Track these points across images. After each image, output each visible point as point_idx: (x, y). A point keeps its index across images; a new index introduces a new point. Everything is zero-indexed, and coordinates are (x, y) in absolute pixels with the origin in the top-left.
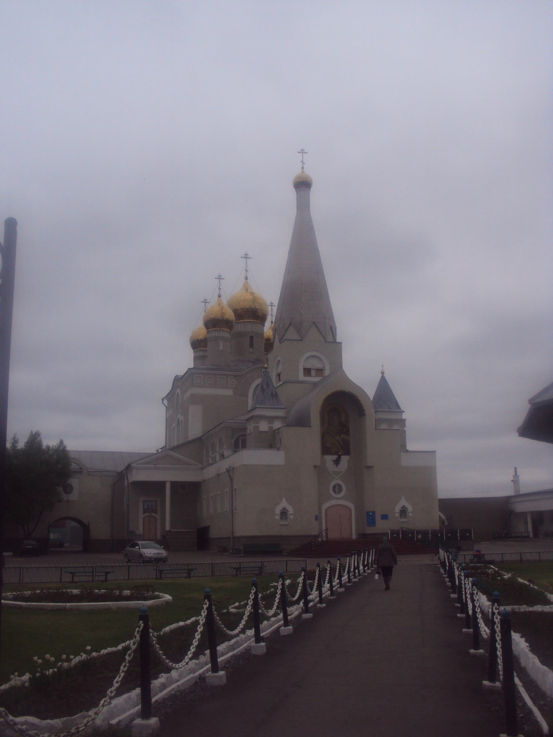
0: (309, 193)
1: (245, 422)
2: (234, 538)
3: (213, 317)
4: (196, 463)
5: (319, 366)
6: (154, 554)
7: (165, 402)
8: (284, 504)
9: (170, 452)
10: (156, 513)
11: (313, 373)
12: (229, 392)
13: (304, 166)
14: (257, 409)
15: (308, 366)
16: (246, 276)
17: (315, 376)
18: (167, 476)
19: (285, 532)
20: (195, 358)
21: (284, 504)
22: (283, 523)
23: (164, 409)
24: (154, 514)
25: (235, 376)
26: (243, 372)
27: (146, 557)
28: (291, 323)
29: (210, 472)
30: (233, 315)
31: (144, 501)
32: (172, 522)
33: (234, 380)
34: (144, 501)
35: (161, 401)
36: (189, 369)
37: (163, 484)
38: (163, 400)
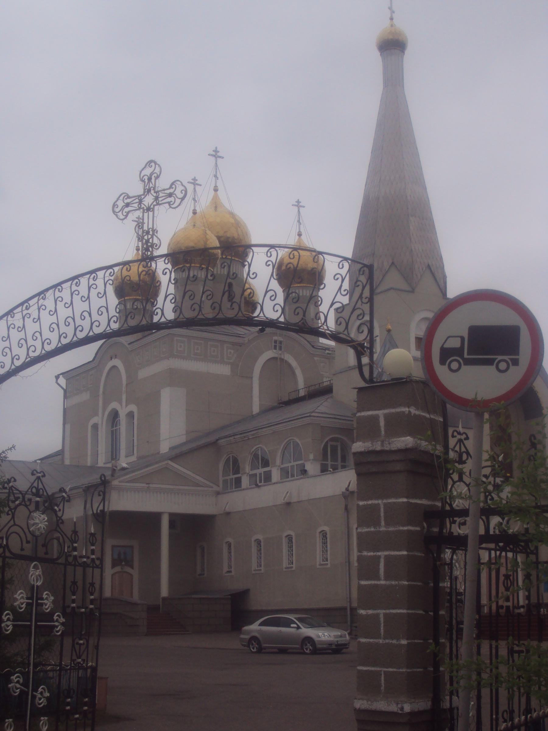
3: (192, 244)
4: (208, 483)
6: (336, 636)
7: (62, 381)
9: (170, 462)
10: (132, 567)
12: (224, 370)
13: (394, 16)
16: (216, 186)
23: (62, 392)
25: (234, 344)
27: (322, 642)
28: (393, 263)
31: (113, 547)
32: (172, 582)
33: (232, 351)
34: (113, 547)
35: (55, 380)
37: (155, 517)
38: (57, 377)
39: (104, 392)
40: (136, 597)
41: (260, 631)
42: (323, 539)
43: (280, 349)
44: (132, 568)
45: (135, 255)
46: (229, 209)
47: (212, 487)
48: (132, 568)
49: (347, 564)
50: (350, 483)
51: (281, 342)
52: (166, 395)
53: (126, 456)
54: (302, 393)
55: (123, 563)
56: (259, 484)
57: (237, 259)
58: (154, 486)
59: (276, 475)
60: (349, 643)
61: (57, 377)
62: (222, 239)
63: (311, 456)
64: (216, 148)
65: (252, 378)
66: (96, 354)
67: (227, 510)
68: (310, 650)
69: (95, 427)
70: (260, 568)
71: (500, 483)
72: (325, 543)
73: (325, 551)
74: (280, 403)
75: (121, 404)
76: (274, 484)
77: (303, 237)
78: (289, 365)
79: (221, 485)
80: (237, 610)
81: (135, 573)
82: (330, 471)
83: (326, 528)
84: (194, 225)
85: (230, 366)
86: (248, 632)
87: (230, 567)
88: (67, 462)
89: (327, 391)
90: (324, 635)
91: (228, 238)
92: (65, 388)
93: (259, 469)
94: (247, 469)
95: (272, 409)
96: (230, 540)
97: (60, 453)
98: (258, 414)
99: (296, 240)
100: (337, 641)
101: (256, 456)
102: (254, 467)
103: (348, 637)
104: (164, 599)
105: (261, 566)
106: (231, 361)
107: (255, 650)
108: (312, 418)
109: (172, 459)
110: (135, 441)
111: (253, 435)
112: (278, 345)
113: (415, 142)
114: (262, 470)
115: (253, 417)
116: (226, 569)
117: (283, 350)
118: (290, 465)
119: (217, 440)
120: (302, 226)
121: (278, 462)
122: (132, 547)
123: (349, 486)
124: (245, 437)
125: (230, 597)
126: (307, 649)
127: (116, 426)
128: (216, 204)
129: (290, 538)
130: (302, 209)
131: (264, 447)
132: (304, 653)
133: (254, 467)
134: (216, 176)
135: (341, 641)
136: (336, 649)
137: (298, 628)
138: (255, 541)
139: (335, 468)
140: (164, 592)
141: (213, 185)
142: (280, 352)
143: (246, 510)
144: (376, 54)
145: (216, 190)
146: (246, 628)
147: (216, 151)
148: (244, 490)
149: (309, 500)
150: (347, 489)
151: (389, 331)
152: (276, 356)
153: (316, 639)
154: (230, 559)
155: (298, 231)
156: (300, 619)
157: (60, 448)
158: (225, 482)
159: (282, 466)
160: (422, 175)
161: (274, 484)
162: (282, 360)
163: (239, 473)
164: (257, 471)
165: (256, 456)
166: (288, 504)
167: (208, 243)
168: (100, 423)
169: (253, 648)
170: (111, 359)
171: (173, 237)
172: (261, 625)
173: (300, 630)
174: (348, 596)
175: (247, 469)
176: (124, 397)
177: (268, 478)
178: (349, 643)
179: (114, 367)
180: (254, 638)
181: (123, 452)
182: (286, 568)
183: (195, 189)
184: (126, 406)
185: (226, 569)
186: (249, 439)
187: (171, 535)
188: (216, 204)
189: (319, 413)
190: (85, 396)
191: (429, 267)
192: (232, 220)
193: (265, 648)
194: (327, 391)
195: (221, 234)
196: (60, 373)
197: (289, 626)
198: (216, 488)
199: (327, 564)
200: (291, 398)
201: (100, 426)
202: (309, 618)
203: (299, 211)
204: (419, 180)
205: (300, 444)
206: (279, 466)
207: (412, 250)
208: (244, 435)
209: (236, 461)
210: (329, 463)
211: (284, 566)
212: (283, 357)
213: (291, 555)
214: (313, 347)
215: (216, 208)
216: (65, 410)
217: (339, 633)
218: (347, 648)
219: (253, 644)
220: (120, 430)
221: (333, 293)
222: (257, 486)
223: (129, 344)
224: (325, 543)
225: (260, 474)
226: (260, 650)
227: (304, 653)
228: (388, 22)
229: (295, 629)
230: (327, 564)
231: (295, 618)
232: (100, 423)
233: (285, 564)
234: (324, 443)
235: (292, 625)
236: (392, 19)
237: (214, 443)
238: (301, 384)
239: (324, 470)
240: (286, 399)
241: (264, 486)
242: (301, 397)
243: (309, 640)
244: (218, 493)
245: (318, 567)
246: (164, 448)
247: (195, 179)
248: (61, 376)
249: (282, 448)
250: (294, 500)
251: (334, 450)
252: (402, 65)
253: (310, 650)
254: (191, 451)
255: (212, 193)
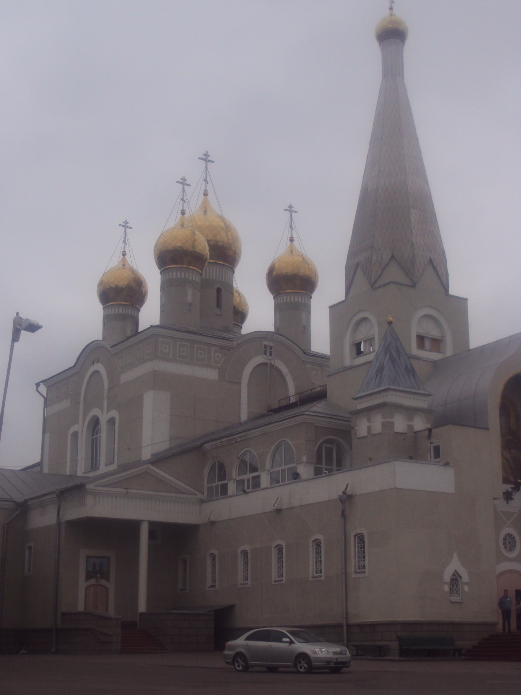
0: (402, 50)
1: (350, 416)
2: (349, 626)
3: (179, 244)
4: (192, 490)
5: (435, 333)
6: (335, 653)
7: (43, 389)
8: (455, 565)
9: (151, 466)
10: (108, 579)
11: (427, 344)
12: (212, 374)
13: (394, 6)
14: (391, 392)
15: (422, 332)
16: (206, 191)
17: (430, 351)
18: (143, 509)
19: (456, 615)
20: (107, 319)
21: (455, 565)
22: (455, 598)
23: (42, 400)
24: (103, 582)
26: (235, 343)
28: (393, 257)
29: (239, 506)
30: (207, 248)
32: (150, 598)
33: (220, 355)
34: (88, 557)
35: (35, 387)
36: (152, 327)
37: (133, 526)
38: (38, 385)
39: (85, 399)
40: (111, 612)
41: (246, 647)
42: (316, 549)
43: (271, 354)
44: (108, 581)
45: (122, 260)
46: (220, 214)
47: (196, 495)
48: (108, 581)
49: (344, 575)
50: (347, 486)
51: (271, 348)
52: (149, 399)
53: (106, 465)
54: (293, 400)
55: (98, 575)
56: (247, 491)
57: (226, 264)
58: (133, 491)
59: (265, 480)
60: (350, 661)
61: (38, 385)
62: (211, 243)
63: (304, 459)
64: (207, 152)
65: (240, 383)
66: (78, 360)
67: (212, 518)
68: (305, 668)
69: (75, 435)
70: (247, 582)
71: (510, 490)
72: (318, 553)
73: (318, 562)
74: (269, 411)
75: (102, 411)
76: (263, 489)
77: (295, 243)
78: (280, 372)
79: (206, 492)
80: (222, 625)
81: (111, 586)
82: (325, 473)
83: (320, 537)
84: (182, 226)
85: (217, 370)
86: (232, 648)
87: (214, 581)
88: (46, 470)
89: (321, 396)
90: (321, 651)
91: (217, 242)
92: (45, 395)
93: (246, 474)
94: (234, 474)
95: (263, 416)
96: (214, 551)
97: (39, 465)
98: (246, 422)
99: (288, 246)
100: (337, 659)
101: (243, 462)
102: (242, 471)
103: (349, 655)
104: (142, 615)
105: (247, 579)
106: (219, 365)
107: (241, 668)
108: (305, 416)
109: (152, 463)
110: (116, 449)
111: (241, 437)
112: (268, 350)
113: (415, 133)
114: (251, 475)
115: (241, 424)
116: (209, 583)
117: (273, 355)
118: (280, 469)
119: (202, 444)
120: (294, 232)
121: (268, 465)
122: (108, 558)
123: (346, 489)
124: (232, 440)
125: (213, 613)
126: (301, 667)
127: (97, 434)
128: (205, 209)
129: (279, 549)
130: (294, 215)
131: (253, 450)
132: (298, 672)
133: (242, 471)
134: (206, 180)
135: (342, 658)
136: (335, 668)
137: (291, 642)
138: (242, 552)
139: (330, 471)
140: (142, 607)
141: (203, 189)
142: (270, 358)
143: (233, 519)
144: (376, 44)
145: (206, 194)
146: (230, 643)
147: (206, 155)
148: (230, 497)
149: (301, 506)
150: (344, 493)
151: (390, 323)
152: (266, 361)
153: (312, 655)
154: (214, 573)
155: (290, 236)
156: (291, 633)
157: (38, 460)
158: (210, 489)
159: (272, 470)
160: (423, 166)
161: (263, 489)
162: (272, 366)
163: (225, 480)
164: (245, 477)
165: (243, 462)
166: (279, 511)
167: (196, 243)
168: (80, 430)
169: (239, 666)
170: (93, 364)
171: (160, 236)
172: (247, 639)
173: (293, 645)
174: (344, 612)
175: (234, 474)
176: (105, 402)
177: (256, 484)
178: (350, 661)
179: (96, 372)
180: (239, 655)
181: (103, 459)
182: (275, 581)
183: (183, 188)
184: (108, 412)
185: (209, 583)
186: (236, 442)
187: (150, 545)
188: (205, 209)
189: (314, 412)
190: (66, 404)
191: (431, 261)
192: (222, 224)
193: (253, 666)
194: (321, 396)
195: (210, 238)
196: (40, 380)
197: (281, 641)
198: (200, 496)
199: (321, 576)
200: (282, 405)
201: (79, 435)
202: (302, 631)
203: (291, 215)
204: (420, 171)
205: (292, 446)
206: (269, 470)
207: (413, 243)
208: (232, 438)
209: (222, 467)
210: (324, 466)
211: (273, 579)
212: (273, 363)
213: (280, 566)
214: (305, 353)
215: (205, 212)
216: (45, 419)
217: (338, 649)
218: (348, 667)
219: (238, 662)
220: (100, 439)
221: (330, 290)
222: (245, 492)
223: (112, 347)
224: (318, 553)
225: (248, 480)
226: (246, 669)
227: (298, 672)
228: (388, 12)
229: (288, 644)
230: (321, 576)
231: (288, 631)
232: (80, 430)
233: (274, 576)
234: (318, 444)
235: (284, 639)
236: (391, 9)
237: (200, 447)
238: (292, 390)
239: (318, 472)
240: (276, 406)
241: (252, 492)
242: (292, 403)
243: (303, 656)
244: (202, 501)
245: (311, 579)
246: (146, 454)
247: (184, 179)
248: (42, 384)
249: (272, 450)
250: (285, 506)
251: (329, 453)
252: (402, 55)
253: (305, 668)
254: (173, 456)
255: (202, 197)
